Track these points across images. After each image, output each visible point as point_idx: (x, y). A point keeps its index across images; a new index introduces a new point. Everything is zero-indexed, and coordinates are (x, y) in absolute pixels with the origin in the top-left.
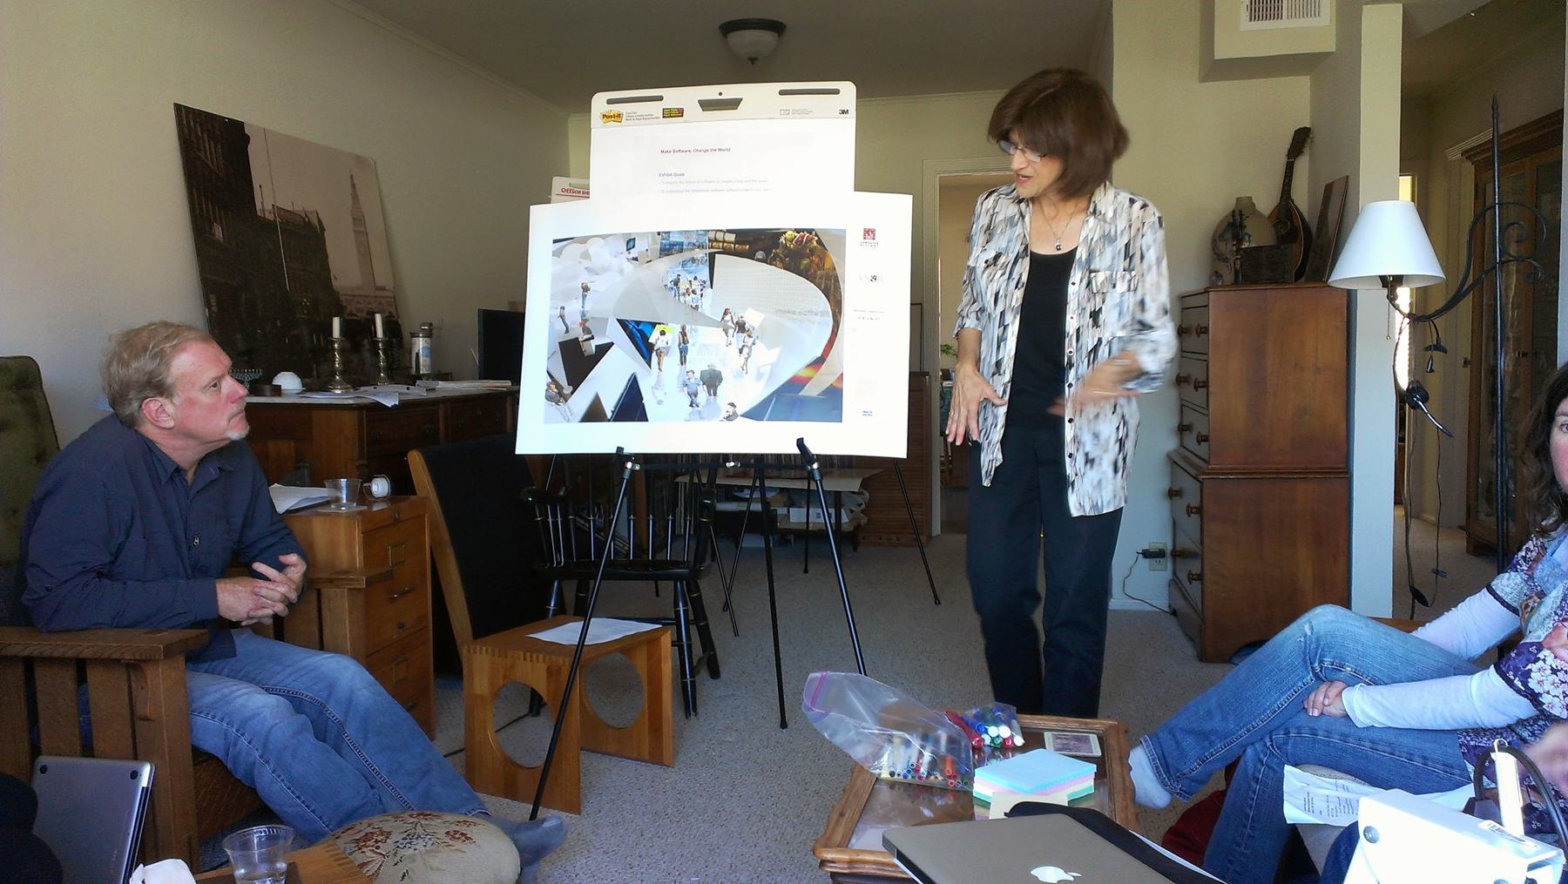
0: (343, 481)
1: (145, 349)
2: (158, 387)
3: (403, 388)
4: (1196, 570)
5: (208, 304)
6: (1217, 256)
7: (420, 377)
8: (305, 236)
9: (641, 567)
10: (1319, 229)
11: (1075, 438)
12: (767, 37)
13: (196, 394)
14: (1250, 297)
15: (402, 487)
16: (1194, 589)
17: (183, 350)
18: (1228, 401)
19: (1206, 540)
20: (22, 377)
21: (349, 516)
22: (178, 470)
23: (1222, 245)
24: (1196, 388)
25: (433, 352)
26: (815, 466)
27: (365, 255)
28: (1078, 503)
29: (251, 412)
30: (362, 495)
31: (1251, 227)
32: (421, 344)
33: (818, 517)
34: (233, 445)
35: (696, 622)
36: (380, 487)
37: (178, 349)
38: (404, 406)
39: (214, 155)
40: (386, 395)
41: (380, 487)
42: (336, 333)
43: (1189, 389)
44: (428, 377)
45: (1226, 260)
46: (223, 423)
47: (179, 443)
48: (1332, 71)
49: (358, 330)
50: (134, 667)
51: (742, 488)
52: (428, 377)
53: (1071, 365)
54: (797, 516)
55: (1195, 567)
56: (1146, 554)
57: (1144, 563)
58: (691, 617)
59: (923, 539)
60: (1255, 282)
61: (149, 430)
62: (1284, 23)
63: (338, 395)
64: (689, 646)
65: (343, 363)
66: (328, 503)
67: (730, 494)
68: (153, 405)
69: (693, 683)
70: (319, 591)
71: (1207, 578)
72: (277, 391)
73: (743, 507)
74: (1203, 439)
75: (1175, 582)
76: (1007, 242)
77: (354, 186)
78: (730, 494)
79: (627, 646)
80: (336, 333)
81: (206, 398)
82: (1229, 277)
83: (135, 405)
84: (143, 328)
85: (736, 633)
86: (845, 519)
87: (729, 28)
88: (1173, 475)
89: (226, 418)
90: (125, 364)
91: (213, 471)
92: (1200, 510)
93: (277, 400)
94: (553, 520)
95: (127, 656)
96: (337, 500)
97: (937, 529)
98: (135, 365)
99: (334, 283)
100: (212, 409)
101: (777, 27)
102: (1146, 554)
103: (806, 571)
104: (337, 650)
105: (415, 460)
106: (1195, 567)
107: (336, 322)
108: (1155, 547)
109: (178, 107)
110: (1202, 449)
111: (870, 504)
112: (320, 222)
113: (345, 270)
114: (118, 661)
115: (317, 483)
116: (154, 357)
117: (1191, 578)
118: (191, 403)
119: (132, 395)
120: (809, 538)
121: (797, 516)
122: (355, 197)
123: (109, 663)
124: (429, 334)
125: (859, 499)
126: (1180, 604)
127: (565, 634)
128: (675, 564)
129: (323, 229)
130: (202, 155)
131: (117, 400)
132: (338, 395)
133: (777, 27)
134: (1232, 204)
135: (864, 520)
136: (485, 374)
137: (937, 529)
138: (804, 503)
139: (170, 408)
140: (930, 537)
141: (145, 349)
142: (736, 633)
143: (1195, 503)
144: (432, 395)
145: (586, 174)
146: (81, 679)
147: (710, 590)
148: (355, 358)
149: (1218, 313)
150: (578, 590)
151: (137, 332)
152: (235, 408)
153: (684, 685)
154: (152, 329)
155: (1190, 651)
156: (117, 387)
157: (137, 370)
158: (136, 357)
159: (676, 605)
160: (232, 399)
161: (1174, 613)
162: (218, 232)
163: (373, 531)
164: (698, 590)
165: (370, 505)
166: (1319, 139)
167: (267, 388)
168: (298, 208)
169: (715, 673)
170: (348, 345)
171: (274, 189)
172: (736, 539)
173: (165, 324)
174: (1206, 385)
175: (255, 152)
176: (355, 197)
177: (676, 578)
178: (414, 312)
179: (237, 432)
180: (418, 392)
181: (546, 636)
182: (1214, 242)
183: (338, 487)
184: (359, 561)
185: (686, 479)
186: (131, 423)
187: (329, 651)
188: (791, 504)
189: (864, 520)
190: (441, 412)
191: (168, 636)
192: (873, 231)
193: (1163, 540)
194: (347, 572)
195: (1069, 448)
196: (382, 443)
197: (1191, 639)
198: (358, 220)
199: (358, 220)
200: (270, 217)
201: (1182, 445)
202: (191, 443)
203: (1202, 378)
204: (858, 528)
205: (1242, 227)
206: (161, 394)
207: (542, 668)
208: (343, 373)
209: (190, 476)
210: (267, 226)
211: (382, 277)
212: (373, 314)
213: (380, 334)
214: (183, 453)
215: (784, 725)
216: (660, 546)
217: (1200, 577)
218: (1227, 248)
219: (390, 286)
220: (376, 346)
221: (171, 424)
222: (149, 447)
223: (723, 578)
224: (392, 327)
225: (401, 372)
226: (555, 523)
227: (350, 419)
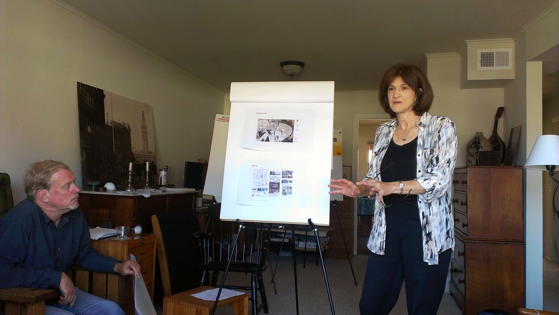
0: (123, 227)
2: (45, 186)
3: (153, 190)
4: (462, 278)
5: (82, 156)
6: (469, 154)
7: (161, 186)
8: (123, 132)
12: (298, 68)
15: (148, 229)
16: (461, 287)
17: (57, 171)
19: (467, 267)
21: (124, 242)
22: (51, 222)
23: (471, 150)
25: (167, 176)
26: (316, 230)
27: (145, 139)
30: (130, 233)
31: (482, 143)
32: (163, 173)
33: (311, 246)
34: (72, 212)
35: (260, 289)
36: (138, 230)
37: (55, 171)
38: (152, 197)
39: (91, 101)
40: (146, 193)
42: (130, 169)
43: (458, 205)
44: (164, 186)
45: (473, 156)
46: (68, 202)
47: (50, 209)
48: (514, 87)
49: (139, 168)
50: (24, 305)
51: (281, 233)
52: (164, 186)
55: (461, 276)
58: (258, 287)
59: (350, 256)
60: (485, 165)
61: (39, 202)
62: (494, 68)
63: (129, 192)
64: (256, 301)
65: (132, 180)
66: (116, 236)
67: (276, 235)
68: (41, 192)
72: (105, 190)
73: (281, 240)
74: (464, 225)
78: (276, 235)
79: (231, 302)
80: (130, 169)
81: (62, 192)
82: (474, 163)
83: (34, 192)
84: (42, 162)
85: (276, 293)
87: (283, 64)
89: (69, 200)
90: (32, 175)
92: (464, 254)
94: (206, 244)
95: (20, 301)
96: (120, 234)
97: (355, 253)
99: (132, 149)
101: (301, 64)
103: (304, 267)
104: (112, 300)
106: (461, 276)
107: (131, 164)
109: (78, 83)
110: (465, 230)
112: (129, 127)
113: (137, 145)
114: (16, 302)
116: (45, 173)
117: (460, 281)
118: (56, 193)
120: (305, 253)
122: (143, 119)
123: (14, 303)
124: (166, 170)
125: (326, 240)
126: (454, 291)
127: (208, 295)
128: (253, 265)
130: (86, 101)
131: (28, 189)
133: (301, 64)
135: (327, 248)
136: (186, 186)
137: (355, 253)
138: (304, 240)
139: (48, 194)
140: (353, 256)
141: (42, 169)
142: (276, 293)
143: (462, 251)
144: (164, 193)
145: (229, 114)
147: (266, 276)
149: (471, 175)
150: (214, 274)
151: (40, 163)
152: (74, 196)
154: (46, 163)
156: (28, 184)
157: (37, 178)
159: (252, 283)
160: (73, 192)
162: (89, 129)
167: (101, 188)
168: (121, 122)
170: (135, 173)
171: (113, 114)
173: (51, 161)
174: (466, 204)
175: (107, 101)
176: (143, 119)
177: (252, 272)
178: (161, 162)
179: (73, 206)
180: (159, 192)
181: (198, 295)
182: (468, 148)
186: (31, 199)
187: (109, 300)
189: (327, 248)
190: (167, 200)
191: (39, 292)
196: (142, 212)
197: (460, 307)
198: (144, 127)
199: (144, 127)
200: (110, 125)
202: (54, 209)
203: (464, 201)
205: (479, 143)
207: (194, 310)
209: (57, 223)
210: (111, 127)
211: (151, 149)
212: (145, 162)
213: (147, 169)
214: (52, 213)
218: (473, 151)
219: (153, 151)
220: (146, 174)
221: (47, 200)
222: (39, 209)
223: (271, 270)
224: (153, 167)
225: (154, 184)
226: (207, 246)
227: (130, 202)
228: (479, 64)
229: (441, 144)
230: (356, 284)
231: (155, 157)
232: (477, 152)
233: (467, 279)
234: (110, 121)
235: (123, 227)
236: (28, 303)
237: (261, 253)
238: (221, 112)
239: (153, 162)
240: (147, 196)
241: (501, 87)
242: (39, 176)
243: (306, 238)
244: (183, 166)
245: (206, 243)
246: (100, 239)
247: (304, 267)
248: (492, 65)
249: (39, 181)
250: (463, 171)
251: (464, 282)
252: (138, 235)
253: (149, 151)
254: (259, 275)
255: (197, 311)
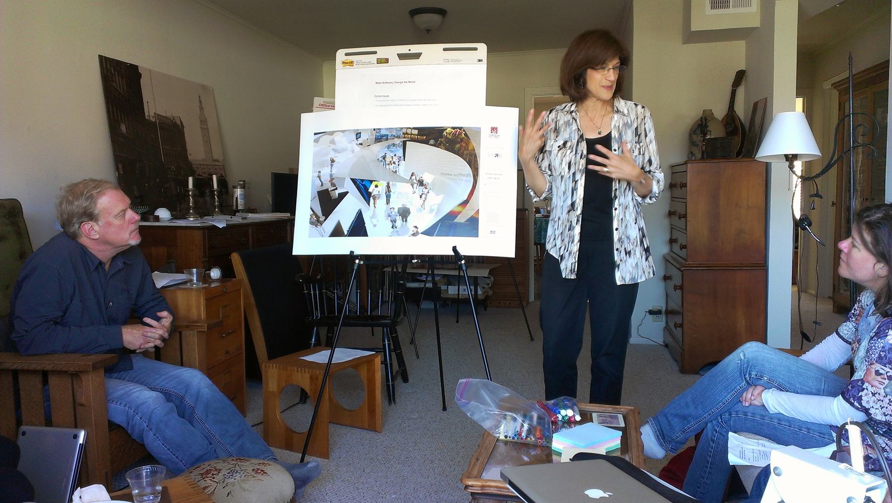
0: (194, 270)
1: (82, 194)
2: (91, 216)
3: (228, 217)
4: (679, 321)
5: (117, 169)
6: (692, 143)
7: (238, 211)
8: (173, 131)
9: (364, 319)
10: (750, 128)
11: (620, 240)
12: (436, 18)
13: (112, 219)
14: (710, 166)
15: (228, 273)
16: (678, 332)
17: (104, 194)
18: (698, 226)
20: (11, 210)
21: (198, 290)
23: (695, 137)
24: (680, 218)
25: (246, 197)
27: (207, 141)
28: (621, 277)
29: (142, 230)
30: (205, 278)
32: (239, 192)
33: (465, 291)
34: (132, 248)
36: (215, 273)
37: (101, 194)
38: (229, 227)
39: (121, 83)
40: (219, 221)
41: (215, 273)
42: (191, 186)
44: (243, 211)
45: (697, 145)
46: (127, 236)
48: (758, 38)
49: (203, 184)
50: (75, 375)
51: (421, 275)
52: (243, 211)
53: (616, 197)
54: (452, 291)
55: (678, 320)
56: (651, 312)
57: (650, 317)
58: (392, 347)
59: (524, 303)
60: (713, 158)
61: (84, 240)
62: (731, 10)
63: (192, 221)
64: (391, 364)
65: (195, 202)
66: (185, 283)
67: (414, 278)
68: (87, 226)
69: (393, 385)
70: (180, 333)
71: (685, 326)
72: (157, 219)
73: (422, 285)
74: (683, 247)
75: (667, 328)
76: (709, 11)
77: (200, 102)
78: (414, 278)
79: (355, 364)
80: (191, 186)
81: (117, 222)
82: (699, 156)
83: (77, 226)
84: (80, 183)
85: (418, 357)
86: (480, 292)
87: (414, 12)
88: (666, 268)
89: (128, 233)
90: (70, 203)
91: (120, 264)
92: (681, 288)
93: (157, 224)
94: (314, 292)
96: (191, 281)
98: (76, 203)
99: (190, 157)
100: (121, 227)
101: (442, 12)
102: (651, 312)
103: (457, 322)
104: (191, 366)
105: (236, 258)
106: (678, 320)
107: (191, 179)
108: (656, 308)
109: (103, 60)
110: (683, 253)
111: (493, 284)
113: (196, 150)
114: (66, 372)
115: (179, 271)
116: (87, 199)
117: (676, 326)
118: (109, 224)
119: (75, 220)
120: (459, 303)
121: (452, 291)
122: (201, 109)
123: (60, 373)
124: (243, 187)
125: (488, 281)
127: (321, 357)
129: (183, 127)
132: (192, 221)
133: (442, 12)
134: (700, 114)
139: (96, 228)
140: (528, 303)
141: (82, 194)
142: (418, 357)
143: (679, 283)
144: (245, 221)
146: (45, 382)
147: (403, 333)
148: (201, 200)
149: (694, 175)
150: (328, 332)
151: (76, 185)
152: (133, 227)
153: (388, 386)
154: (85, 183)
155: (675, 367)
156: (65, 216)
157: (77, 206)
158: (77, 199)
159: (384, 341)
160: (131, 222)
161: (666, 346)
162: (123, 128)
163: (212, 298)
164: (396, 332)
165: (210, 283)
166: (748, 74)
167: (151, 217)
168: (169, 115)
169: (405, 380)
170: (197, 192)
171: (156, 104)
172: (418, 303)
173: (92, 180)
174: (685, 216)
175: (143, 81)
176: (201, 109)
177: (383, 325)
178: (235, 174)
179: (134, 241)
180: (237, 220)
182: (690, 134)
183: (191, 274)
184: (203, 315)
185: (389, 269)
187: (186, 366)
188: (449, 284)
189: (490, 293)
190: (250, 232)
191: (93, 358)
192: (496, 129)
193: (661, 304)
194: (196, 322)
195: (616, 245)
196: (216, 249)
197: (676, 361)
198: (203, 122)
199: (203, 122)
200: (153, 120)
201: (671, 251)
202: (109, 247)
203: (683, 213)
204: (487, 297)
205: (706, 126)
206: (91, 220)
207: (307, 376)
208: (194, 209)
209: (107, 267)
210: (154, 124)
212: (212, 175)
213: (215, 186)
214: (103, 254)
215: (445, 409)
216: (375, 307)
217: (681, 326)
218: (698, 138)
219: (221, 159)
221: (97, 237)
222: (83, 249)
224: (223, 182)
225: (228, 208)
226: (315, 295)
227: (198, 235)
228: (708, 5)
229: (638, 135)
230: (532, 339)
231: (223, 168)
232: (703, 141)
233: (685, 322)
234: (152, 114)
235: (194, 270)
236: (81, 372)
237: (393, 306)
238: (321, 95)
239: (222, 176)
240: (221, 225)
241: (742, 39)
242: (80, 204)
243: (459, 280)
244: (268, 181)
245: (315, 290)
246: (163, 287)
247: (457, 322)
248: (728, 7)
249: (81, 211)
250: (682, 168)
251: (681, 326)
252: (217, 280)
253: (215, 157)
254: (393, 330)
255: (311, 378)
